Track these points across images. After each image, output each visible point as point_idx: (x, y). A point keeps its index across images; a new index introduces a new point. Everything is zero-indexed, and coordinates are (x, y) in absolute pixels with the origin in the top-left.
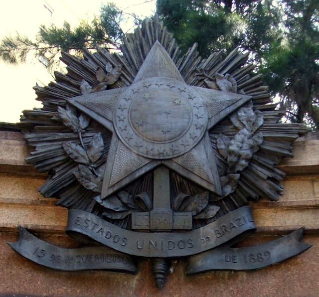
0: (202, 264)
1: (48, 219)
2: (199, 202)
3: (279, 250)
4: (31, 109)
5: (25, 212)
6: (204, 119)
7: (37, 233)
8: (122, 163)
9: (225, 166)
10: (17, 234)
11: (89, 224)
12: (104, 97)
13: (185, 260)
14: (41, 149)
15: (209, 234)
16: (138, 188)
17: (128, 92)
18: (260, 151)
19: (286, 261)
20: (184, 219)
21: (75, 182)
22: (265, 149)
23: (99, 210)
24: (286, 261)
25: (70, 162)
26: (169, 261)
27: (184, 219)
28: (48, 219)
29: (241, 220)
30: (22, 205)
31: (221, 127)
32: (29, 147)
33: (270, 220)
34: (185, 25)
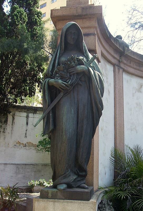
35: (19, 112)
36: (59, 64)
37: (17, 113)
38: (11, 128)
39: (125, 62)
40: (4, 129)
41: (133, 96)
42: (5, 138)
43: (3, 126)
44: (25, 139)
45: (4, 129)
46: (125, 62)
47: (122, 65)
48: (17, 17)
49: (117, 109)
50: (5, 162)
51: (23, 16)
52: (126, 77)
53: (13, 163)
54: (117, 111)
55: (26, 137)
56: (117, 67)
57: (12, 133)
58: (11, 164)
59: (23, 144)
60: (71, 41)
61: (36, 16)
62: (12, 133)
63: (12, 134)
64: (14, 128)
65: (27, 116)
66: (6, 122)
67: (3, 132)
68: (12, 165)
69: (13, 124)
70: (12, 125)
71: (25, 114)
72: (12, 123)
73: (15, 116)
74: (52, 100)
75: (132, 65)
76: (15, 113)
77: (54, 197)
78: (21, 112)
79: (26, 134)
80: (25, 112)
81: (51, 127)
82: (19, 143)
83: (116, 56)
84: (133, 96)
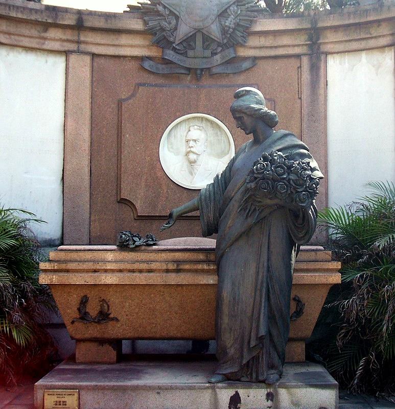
0: (214, 71)
1: (154, 52)
2: (213, 46)
3: (246, 65)
7: (149, 58)
8: (183, 30)
9: (224, 31)
11: (170, 55)
14: (151, 24)
15: (218, 59)
16: (189, 41)
18: (238, 25)
23: (174, 49)
25: (162, 29)
26: (202, 70)
27: (208, 53)
28: (154, 52)
29: (230, 54)
30: (144, 47)
32: (146, 23)
33: (243, 52)
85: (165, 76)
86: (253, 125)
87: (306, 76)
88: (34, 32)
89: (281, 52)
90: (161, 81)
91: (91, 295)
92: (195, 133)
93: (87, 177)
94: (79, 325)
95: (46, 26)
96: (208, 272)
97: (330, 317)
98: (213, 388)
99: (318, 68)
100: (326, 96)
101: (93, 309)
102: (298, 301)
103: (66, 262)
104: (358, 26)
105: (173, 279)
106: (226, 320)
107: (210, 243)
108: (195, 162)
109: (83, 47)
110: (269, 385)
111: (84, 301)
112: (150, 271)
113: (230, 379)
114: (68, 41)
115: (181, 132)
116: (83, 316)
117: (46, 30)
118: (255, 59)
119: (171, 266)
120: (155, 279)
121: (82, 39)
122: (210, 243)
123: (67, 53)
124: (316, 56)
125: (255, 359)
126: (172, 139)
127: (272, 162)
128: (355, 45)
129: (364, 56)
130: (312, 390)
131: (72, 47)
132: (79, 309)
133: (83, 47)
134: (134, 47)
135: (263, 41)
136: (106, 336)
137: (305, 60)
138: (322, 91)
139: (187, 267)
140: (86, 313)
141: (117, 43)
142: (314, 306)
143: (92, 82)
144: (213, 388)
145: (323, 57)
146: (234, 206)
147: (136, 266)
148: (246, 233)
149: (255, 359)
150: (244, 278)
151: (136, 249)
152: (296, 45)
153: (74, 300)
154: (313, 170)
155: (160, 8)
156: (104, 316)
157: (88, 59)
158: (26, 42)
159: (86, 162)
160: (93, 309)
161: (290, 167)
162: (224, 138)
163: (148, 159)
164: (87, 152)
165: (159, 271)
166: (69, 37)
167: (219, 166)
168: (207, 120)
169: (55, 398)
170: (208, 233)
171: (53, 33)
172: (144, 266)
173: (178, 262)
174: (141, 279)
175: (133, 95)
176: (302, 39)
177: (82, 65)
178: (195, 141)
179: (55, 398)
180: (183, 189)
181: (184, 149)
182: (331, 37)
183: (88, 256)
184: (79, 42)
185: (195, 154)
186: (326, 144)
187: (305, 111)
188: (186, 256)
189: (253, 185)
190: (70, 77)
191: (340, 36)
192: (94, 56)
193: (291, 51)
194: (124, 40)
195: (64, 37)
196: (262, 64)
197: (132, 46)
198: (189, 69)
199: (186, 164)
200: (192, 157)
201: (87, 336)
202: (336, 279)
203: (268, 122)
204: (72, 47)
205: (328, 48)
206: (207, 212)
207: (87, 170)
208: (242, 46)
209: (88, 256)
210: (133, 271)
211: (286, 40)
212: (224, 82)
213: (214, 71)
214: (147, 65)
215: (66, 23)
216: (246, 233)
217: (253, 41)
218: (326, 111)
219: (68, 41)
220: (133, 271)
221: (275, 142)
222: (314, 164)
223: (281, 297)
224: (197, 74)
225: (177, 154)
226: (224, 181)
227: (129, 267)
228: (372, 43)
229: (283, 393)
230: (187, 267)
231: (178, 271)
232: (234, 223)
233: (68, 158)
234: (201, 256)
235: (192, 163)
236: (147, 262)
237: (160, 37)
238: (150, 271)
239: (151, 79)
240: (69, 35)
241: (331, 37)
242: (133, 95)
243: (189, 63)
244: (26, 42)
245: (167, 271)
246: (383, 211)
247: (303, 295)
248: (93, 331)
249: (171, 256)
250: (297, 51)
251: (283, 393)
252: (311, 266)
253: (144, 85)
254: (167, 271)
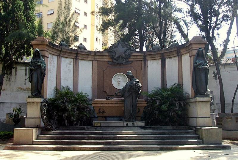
0: (124, 64)
1: (111, 60)
2: (123, 59)
3: (130, 62)
4: (237, 31)
5: (54, 85)
6: (124, 51)
7: (109, 61)
8: (117, 56)
9: (126, 56)
10: (108, 61)
11: (114, 61)
12: (115, 49)
13: (123, 63)
14: (110, 54)
15: (124, 61)
16: (118, 58)
17: (117, 49)
18: (128, 54)
19: (131, 63)
20: (122, 60)
21: (113, 57)
22: (98, 92)
23: (115, 59)
24: (131, 63)
25: (112, 55)
26: (121, 64)
27: (122, 60)
28: (111, 60)
29: (127, 60)
30: (108, 59)
31: (125, 52)
32: (109, 54)
33: (130, 60)
34: (24, 31)
35: (20, 66)
36: (33, 63)
37: (19, 67)
38: (14, 77)
39: (63, 53)
40: (9, 79)
41: (67, 66)
42: (10, 85)
43: (9, 77)
44: (24, 85)
45: (9, 79)
46: (63, 53)
47: (61, 55)
48: (17, 8)
49: (58, 72)
50: (11, 102)
51: (21, 7)
52: (63, 59)
53: (17, 102)
54: (58, 73)
55: (25, 84)
56: (58, 56)
57: (15, 82)
58: (15, 103)
59: (23, 89)
60: (37, 54)
61: (30, 3)
62: (15, 82)
63: (16, 82)
64: (17, 78)
65: (26, 69)
66: (11, 73)
67: (9, 81)
68: (16, 104)
69: (16, 75)
70: (15, 76)
71: (24, 68)
72: (15, 74)
73: (17, 70)
74: (31, 73)
75: (66, 54)
76: (17, 67)
77: (31, 97)
78: (21, 66)
79: (25, 82)
80: (24, 66)
81: (31, 80)
82: (21, 89)
83: (58, 52)
84: (67, 66)
85: (113, 65)
86: (130, 78)
87: (143, 65)
88: (86, 57)
89: (138, 60)
90: (113, 66)
91: (101, 108)
92: (120, 77)
93: (97, 87)
94: (99, 114)
95: (88, 55)
96: (122, 104)
97: (145, 112)
98: (123, 122)
99: (146, 63)
100: (147, 69)
101: (101, 111)
102: (139, 109)
103: (97, 102)
104: (154, 54)
105: (116, 105)
106: (125, 111)
107: (123, 99)
108: (119, 83)
109: (96, 59)
110: (133, 122)
111: (100, 109)
112: (112, 103)
113: (126, 121)
114: (93, 58)
115: (117, 77)
116: (100, 112)
117: (88, 56)
118: (132, 61)
119: (116, 103)
120: (113, 105)
121: (96, 57)
122: (123, 99)
123: (92, 61)
124: (145, 61)
125: (130, 117)
126: (115, 78)
127: (133, 84)
128: (153, 59)
129: (155, 61)
130: (140, 123)
131: (94, 59)
132: (99, 111)
133: (96, 59)
134: (106, 59)
135: (134, 57)
136: (104, 116)
137: (143, 61)
138: (146, 68)
139: (119, 103)
140: (100, 111)
141: (103, 58)
142: (142, 110)
143: (98, 66)
144: (123, 122)
145: (147, 61)
146: (126, 92)
147: (109, 103)
148: (129, 96)
149: (130, 117)
150: (128, 103)
151: (109, 100)
152: (141, 58)
153: (98, 108)
154: (140, 85)
155: (112, 51)
156: (103, 112)
157: (97, 62)
158: (84, 59)
159: (97, 84)
160: (101, 111)
161: (136, 85)
162: (125, 78)
163: (110, 83)
164: (97, 81)
165: (114, 103)
166: (93, 57)
167: (124, 84)
168: (122, 74)
169: (96, 124)
170: (122, 97)
171: (90, 56)
172: (111, 103)
173: (117, 102)
174: (110, 105)
175: (106, 69)
176: (142, 57)
177: (96, 63)
178: (119, 79)
179: (96, 124)
180: (28, 144)
181: (117, 81)
182: (148, 57)
183: (101, 101)
184: (95, 58)
185: (119, 82)
186: (147, 79)
187: (143, 72)
188: (119, 101)
189: (130, 88)
190: (93, 66)
191: (150, 57)
192: (98, 61)
193: (140, 60)
194: (104, 57)
195: (92, 57)
196: (134, 62)
197: (106, 59)
198: (118, 63)
199: (118, 84)
200: (119, 82)
201: (100, 116)
202: (146, 105)
203: (133, 77)
204: (94, 59)
205: (148, 59)
206: (122, 93)
207: (97, 85)
208: (129, 58)
209: (101, 101)
210: (109, 103)
211: (139, 57)
212: (126, 66)
213: (124, 64)
214: (109, 63)
215: (92, 54)
216: (129, 96)
217: (132, 57)
218: (147, 72)
219: (93, 58)
220: (109, 103)
221: (133, 80)
222: (140, 84)
223: (135, 106)
224: (120, 64)
225: (116, 82)
226: (125, 87)
227: (108, 103)
228: (157, 58)
229: (135, 123)
230: (119, 103)
231: (117, 103)
232: (126, 94)
233: (93, 82)
234: (121, 101)
235: (119, 83)
236: (111, 102)
237: (112, 57)
238: (112, 103)
239: (110, 66)
240: (93, 57)
241: (148, 57)
242: (106, 69)
243: (118, 62)
244: (84, 59)
245: (115, 103)
246: (174, 95)
247: (140, 108)
248: (101, 115)
249: (115, 101)
250: (141, 59)
251: (135, 123)
252: (141, 102)
253: (108, 67)
254: (115, 103)
